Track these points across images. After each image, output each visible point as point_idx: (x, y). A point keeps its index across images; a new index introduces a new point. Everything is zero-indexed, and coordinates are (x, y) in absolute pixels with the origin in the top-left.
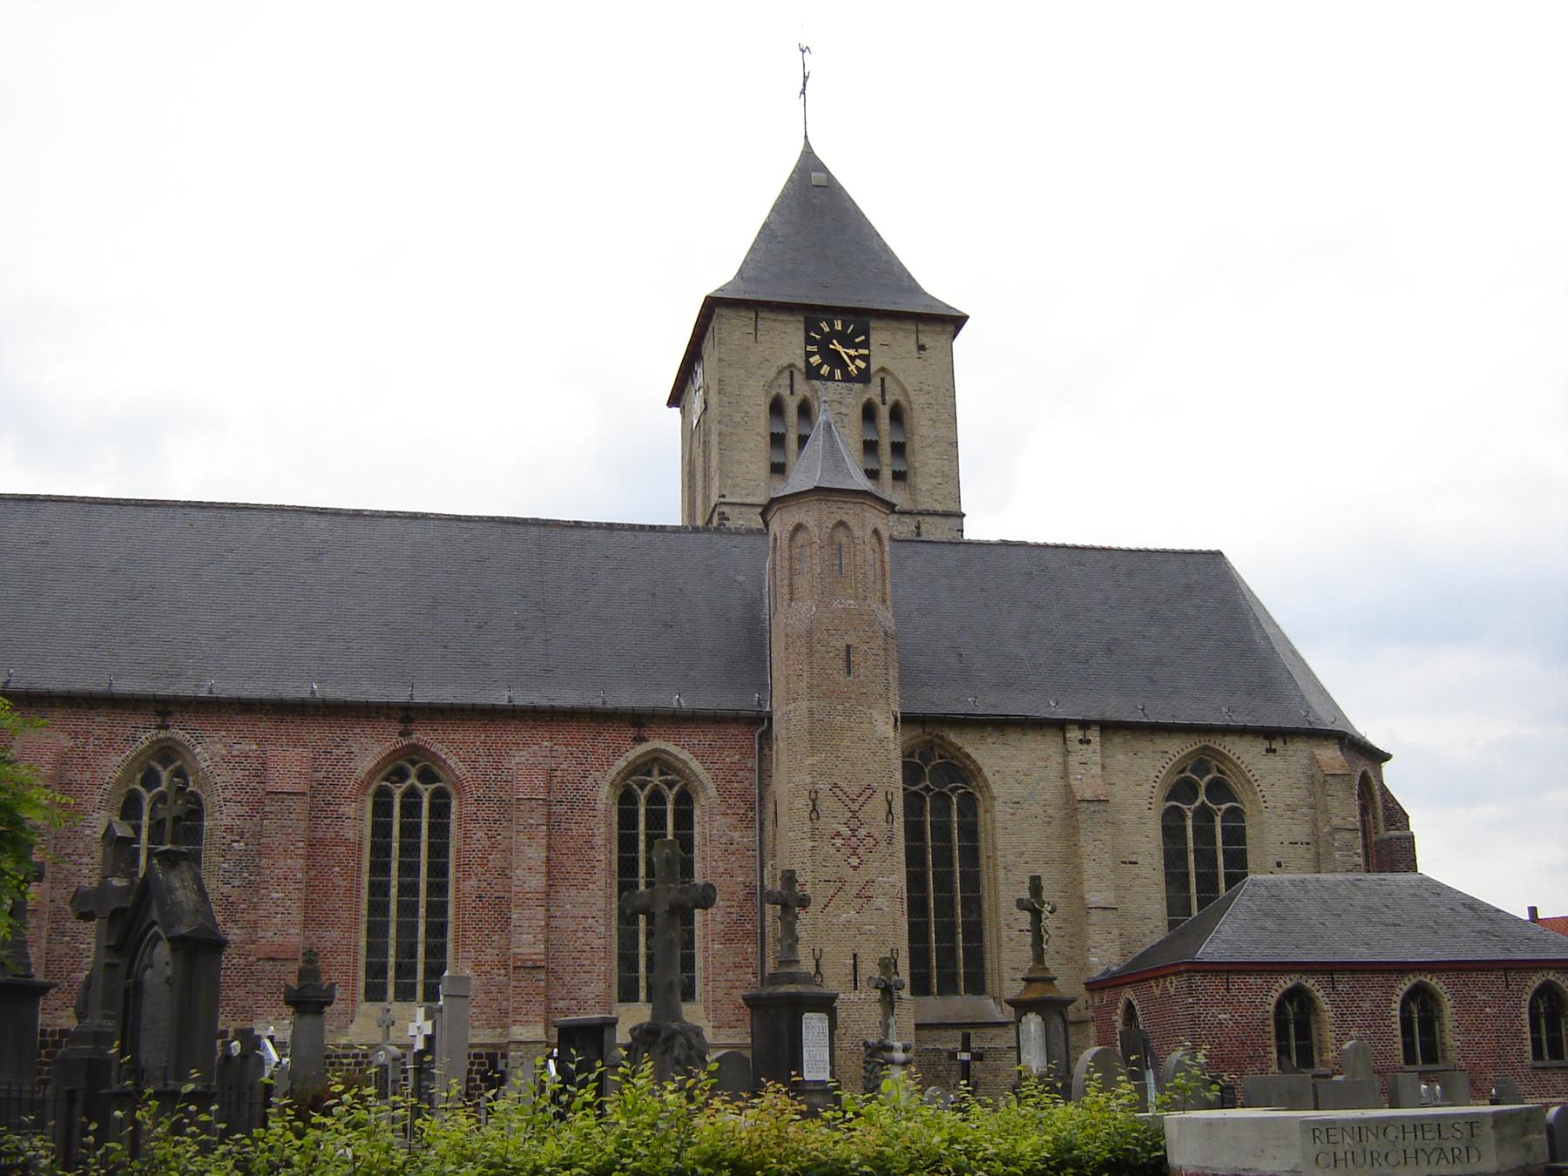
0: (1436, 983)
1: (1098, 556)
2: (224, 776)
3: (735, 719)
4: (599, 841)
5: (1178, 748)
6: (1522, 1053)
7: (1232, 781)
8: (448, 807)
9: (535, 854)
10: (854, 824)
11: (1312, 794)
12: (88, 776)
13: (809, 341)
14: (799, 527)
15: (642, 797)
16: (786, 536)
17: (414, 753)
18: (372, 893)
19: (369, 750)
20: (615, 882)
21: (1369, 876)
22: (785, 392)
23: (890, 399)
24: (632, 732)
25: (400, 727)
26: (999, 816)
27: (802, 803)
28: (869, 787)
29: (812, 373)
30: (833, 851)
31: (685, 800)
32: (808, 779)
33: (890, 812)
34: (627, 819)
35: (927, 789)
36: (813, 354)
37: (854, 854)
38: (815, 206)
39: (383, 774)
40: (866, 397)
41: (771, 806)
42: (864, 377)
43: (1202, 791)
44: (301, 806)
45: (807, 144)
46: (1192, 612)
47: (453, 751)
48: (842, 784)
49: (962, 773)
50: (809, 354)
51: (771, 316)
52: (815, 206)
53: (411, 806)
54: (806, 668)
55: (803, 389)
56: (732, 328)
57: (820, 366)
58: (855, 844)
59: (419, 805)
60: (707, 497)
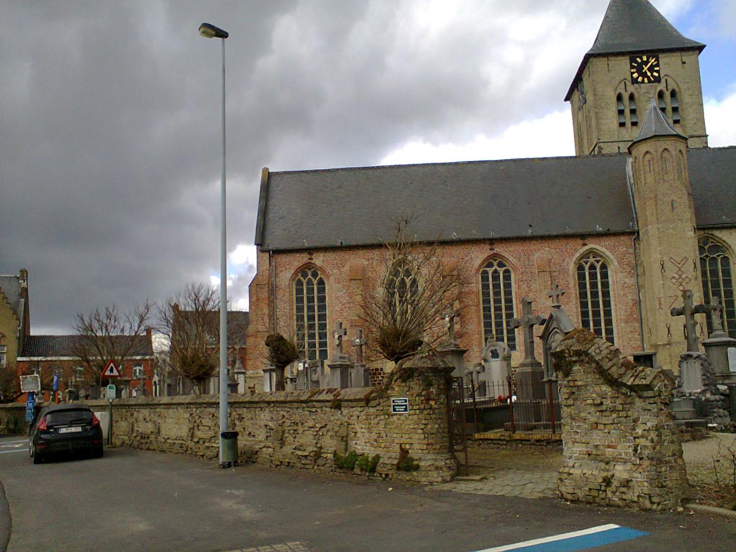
4: (572, 285)
10: (680, 273)
13: (632, 67)
14: (647, 152)
15: (587, 267)
16: (641, 157)
17: (495, 256)
18: (484, 311)
20: (579, 302)
24: (580, 242)
25: (489, 247)
27: (657, 267)
28: (685, 257)
29: (634, 81)
30: (672, 284)
31: (604, 267)
32: (659, 256)
33: (695, 267)
34: (581, 277)
35: (707, 256)
36: (634, 73)
37: (681, 285)
39: (484, 265)
42: (658, 80)
48: (674, 258)
49: (720, 247)
51: (614, 58)
53: (496, 277)
54: (655, 211)
55: (631, 88)
56: (599, 64)
57: (638, 78)
60: (590, 140)
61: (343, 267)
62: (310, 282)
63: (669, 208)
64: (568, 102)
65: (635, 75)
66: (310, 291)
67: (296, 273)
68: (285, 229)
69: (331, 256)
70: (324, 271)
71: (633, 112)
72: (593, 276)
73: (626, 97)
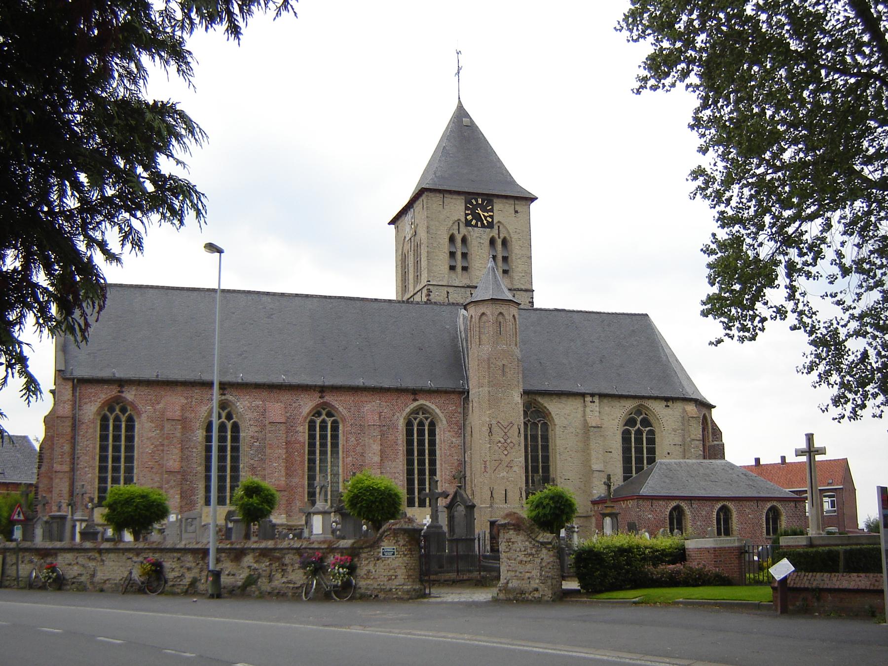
0: (730, 505)
1: (596, 316)
2: (249, 415)
3: (453, 392)
4: (400, 442)
5: (630, 405)
6: (762, 532)
7: (651, 419)
8: (338, 427)
9: (376, 447)
10: (506, 438)
11: (683, 424)
12: (193, 415)
13: (467, 208)
14: (483, 314)
15: (416, 423)
16: (477, 318)
17: (324, 405)
18: (309, 463)
19: (307, 404)
21: (705, 461)
22: (456, 232)
23: (502, 236)
24: (412, 397)
25: (319, 395)
26: (557, 433)
27: (485, 429)
29: (468, 223)
31: (432, 425)
34: (409, 433)
38: (463, 135)
40: (491, 235)
41: (469, 429)
42: (491, 225)
43: (639, 422)
44: (283, 427)
45: (460, 102)
46: (635, 343)
47: (341, 404)
50: (467, 215)
51: (450, 196)
52: (463, 135)
53: (323, 428)
55: (464, 230)
56: (434, 201)
57: (471, 220)
58: (506, 446)
59: (326, 426)
61: (158, 403)
62: (117, 419)
63: (500, 372)
64: (393, 226)
65: (469, 217)
66: (117, 428)
67: (102, 407)
68: (89, 354)
69: (144, 391)
70: (135, 408)
71: (464, 255)
72: (421, 433)
73: (459, 239)
